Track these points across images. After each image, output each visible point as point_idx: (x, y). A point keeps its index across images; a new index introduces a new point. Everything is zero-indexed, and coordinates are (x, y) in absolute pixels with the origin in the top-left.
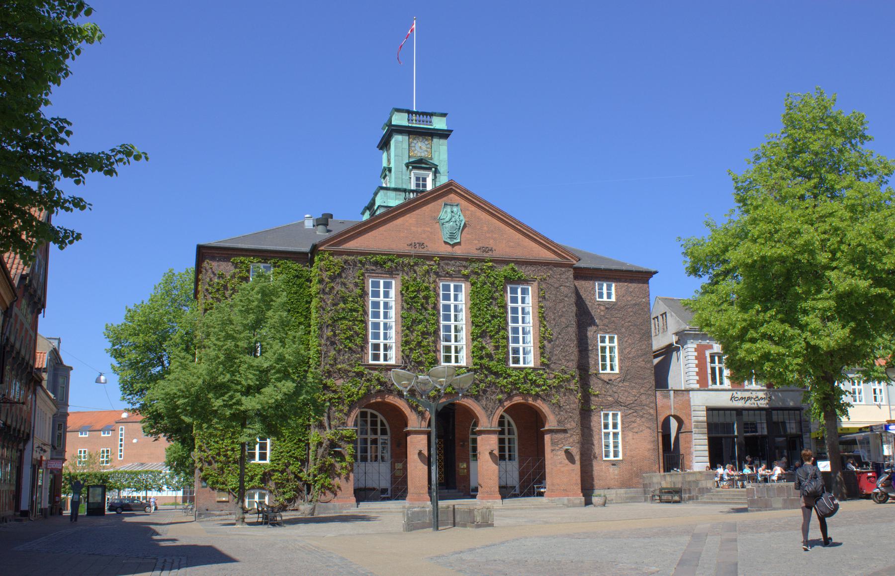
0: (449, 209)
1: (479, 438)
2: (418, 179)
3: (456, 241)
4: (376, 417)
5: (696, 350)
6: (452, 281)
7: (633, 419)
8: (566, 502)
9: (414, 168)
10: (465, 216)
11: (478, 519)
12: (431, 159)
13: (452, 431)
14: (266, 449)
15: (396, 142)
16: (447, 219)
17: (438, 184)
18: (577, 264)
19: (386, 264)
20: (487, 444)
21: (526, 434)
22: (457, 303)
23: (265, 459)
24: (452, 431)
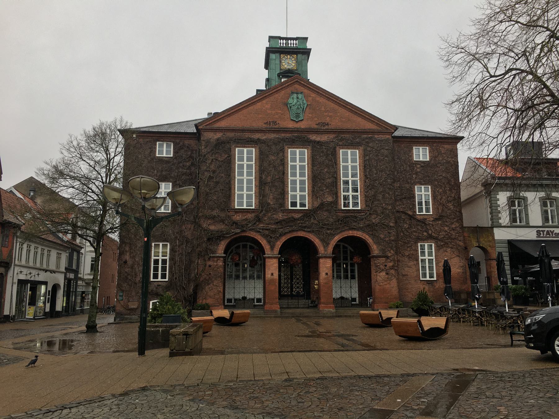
0: (295, 96)
3: (300, 119)
4: (347, 248)
6: (297, 148)
10: (307, 101)
13: (299, 256)
14: (154, 267)
16: (294, 103)
21: (354, 257)
22: (298, 160)
23: (433, 277)
24: (299, 256)
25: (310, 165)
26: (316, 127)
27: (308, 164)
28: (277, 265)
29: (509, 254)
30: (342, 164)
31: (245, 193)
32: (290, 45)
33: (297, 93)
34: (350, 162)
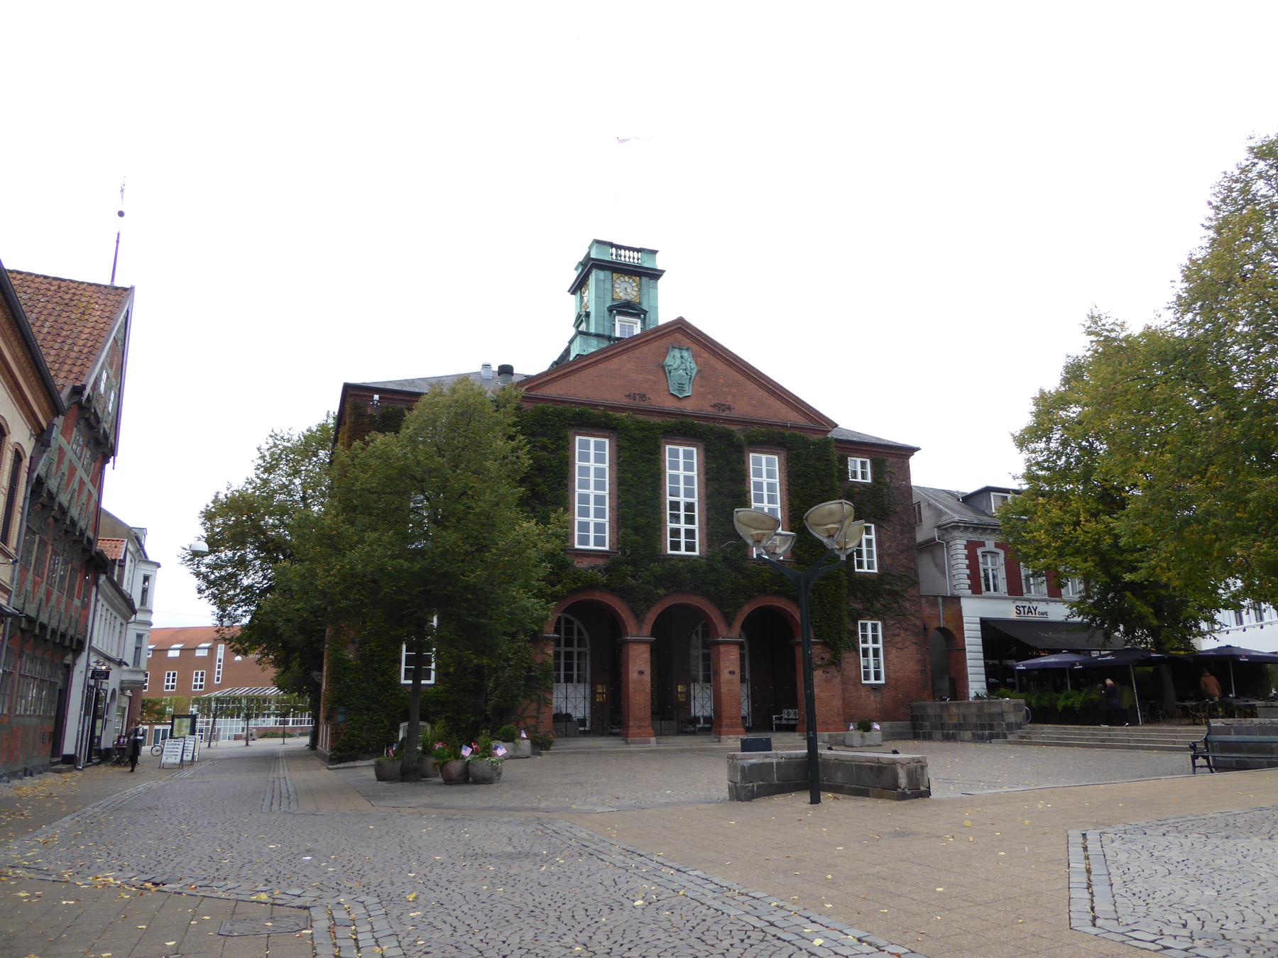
1: (722, 649)
5: (966, 547)
6: (681, 445)
7: (897, 631)
9: (620, 313)
11: (903, 781)
15: (597, 280)
16: (675, 366)
19: (593, 420)
22: (682, 469)
26: (711, 410)
28: (647, 655)
30: (695, 473)
31: (591, 519)
34: (766, 474)
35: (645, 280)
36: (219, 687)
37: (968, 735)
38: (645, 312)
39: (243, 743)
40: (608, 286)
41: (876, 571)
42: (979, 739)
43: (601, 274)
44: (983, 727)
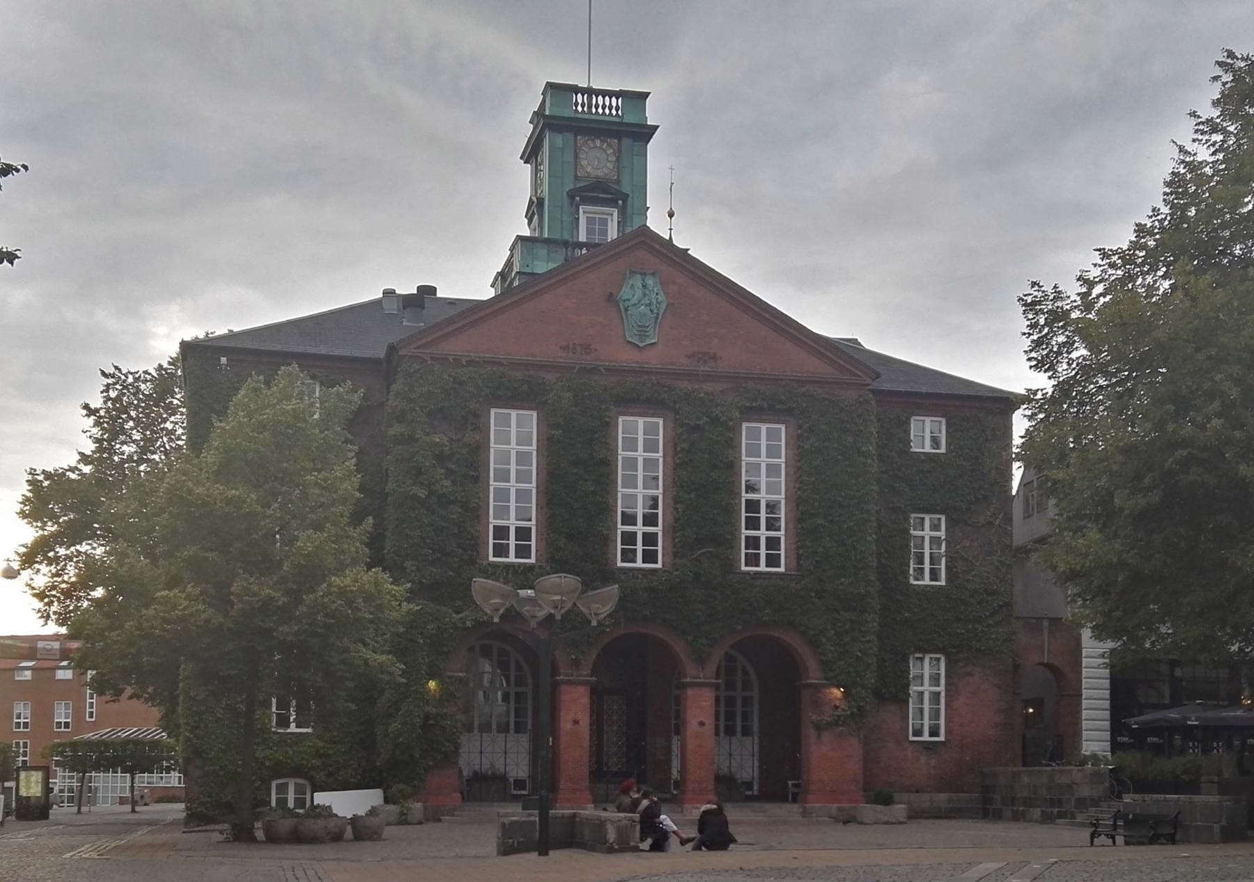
2: (590, 221)
8: (834, 812)
9: (585, 201)
10: (667, 294)
11: (612, 836)
12: (618, 182)
13: (635, 683)
14: (726, 712)
16: (634, 300)
17: (628, 230)
18: (875, 385)
20: (700, 709)
21: (770, 699)
22: (641, 451)
23: (937, 735)
24: (635, 683)
25: (669, 459)
27: (664, 457)
28: (585, 700)
29: (1112, 684)
32: (600, 111)
33: (644, 274)
35: (626, 142)
36: (94, 726)
37: (1036, 813)
38: (625, 197)
39: (128, 808)
40: (569, 157)
41: (943, 583)
42: (1048, 819)
43: (559, 139)
44: (1052, 802)
